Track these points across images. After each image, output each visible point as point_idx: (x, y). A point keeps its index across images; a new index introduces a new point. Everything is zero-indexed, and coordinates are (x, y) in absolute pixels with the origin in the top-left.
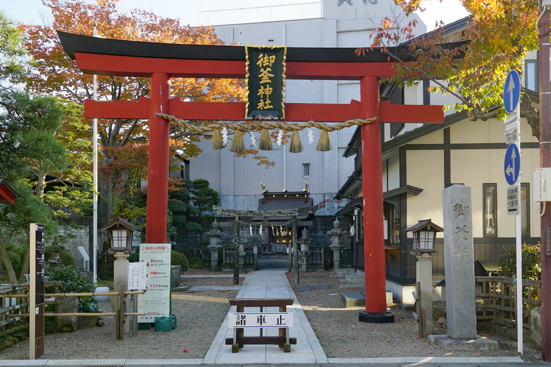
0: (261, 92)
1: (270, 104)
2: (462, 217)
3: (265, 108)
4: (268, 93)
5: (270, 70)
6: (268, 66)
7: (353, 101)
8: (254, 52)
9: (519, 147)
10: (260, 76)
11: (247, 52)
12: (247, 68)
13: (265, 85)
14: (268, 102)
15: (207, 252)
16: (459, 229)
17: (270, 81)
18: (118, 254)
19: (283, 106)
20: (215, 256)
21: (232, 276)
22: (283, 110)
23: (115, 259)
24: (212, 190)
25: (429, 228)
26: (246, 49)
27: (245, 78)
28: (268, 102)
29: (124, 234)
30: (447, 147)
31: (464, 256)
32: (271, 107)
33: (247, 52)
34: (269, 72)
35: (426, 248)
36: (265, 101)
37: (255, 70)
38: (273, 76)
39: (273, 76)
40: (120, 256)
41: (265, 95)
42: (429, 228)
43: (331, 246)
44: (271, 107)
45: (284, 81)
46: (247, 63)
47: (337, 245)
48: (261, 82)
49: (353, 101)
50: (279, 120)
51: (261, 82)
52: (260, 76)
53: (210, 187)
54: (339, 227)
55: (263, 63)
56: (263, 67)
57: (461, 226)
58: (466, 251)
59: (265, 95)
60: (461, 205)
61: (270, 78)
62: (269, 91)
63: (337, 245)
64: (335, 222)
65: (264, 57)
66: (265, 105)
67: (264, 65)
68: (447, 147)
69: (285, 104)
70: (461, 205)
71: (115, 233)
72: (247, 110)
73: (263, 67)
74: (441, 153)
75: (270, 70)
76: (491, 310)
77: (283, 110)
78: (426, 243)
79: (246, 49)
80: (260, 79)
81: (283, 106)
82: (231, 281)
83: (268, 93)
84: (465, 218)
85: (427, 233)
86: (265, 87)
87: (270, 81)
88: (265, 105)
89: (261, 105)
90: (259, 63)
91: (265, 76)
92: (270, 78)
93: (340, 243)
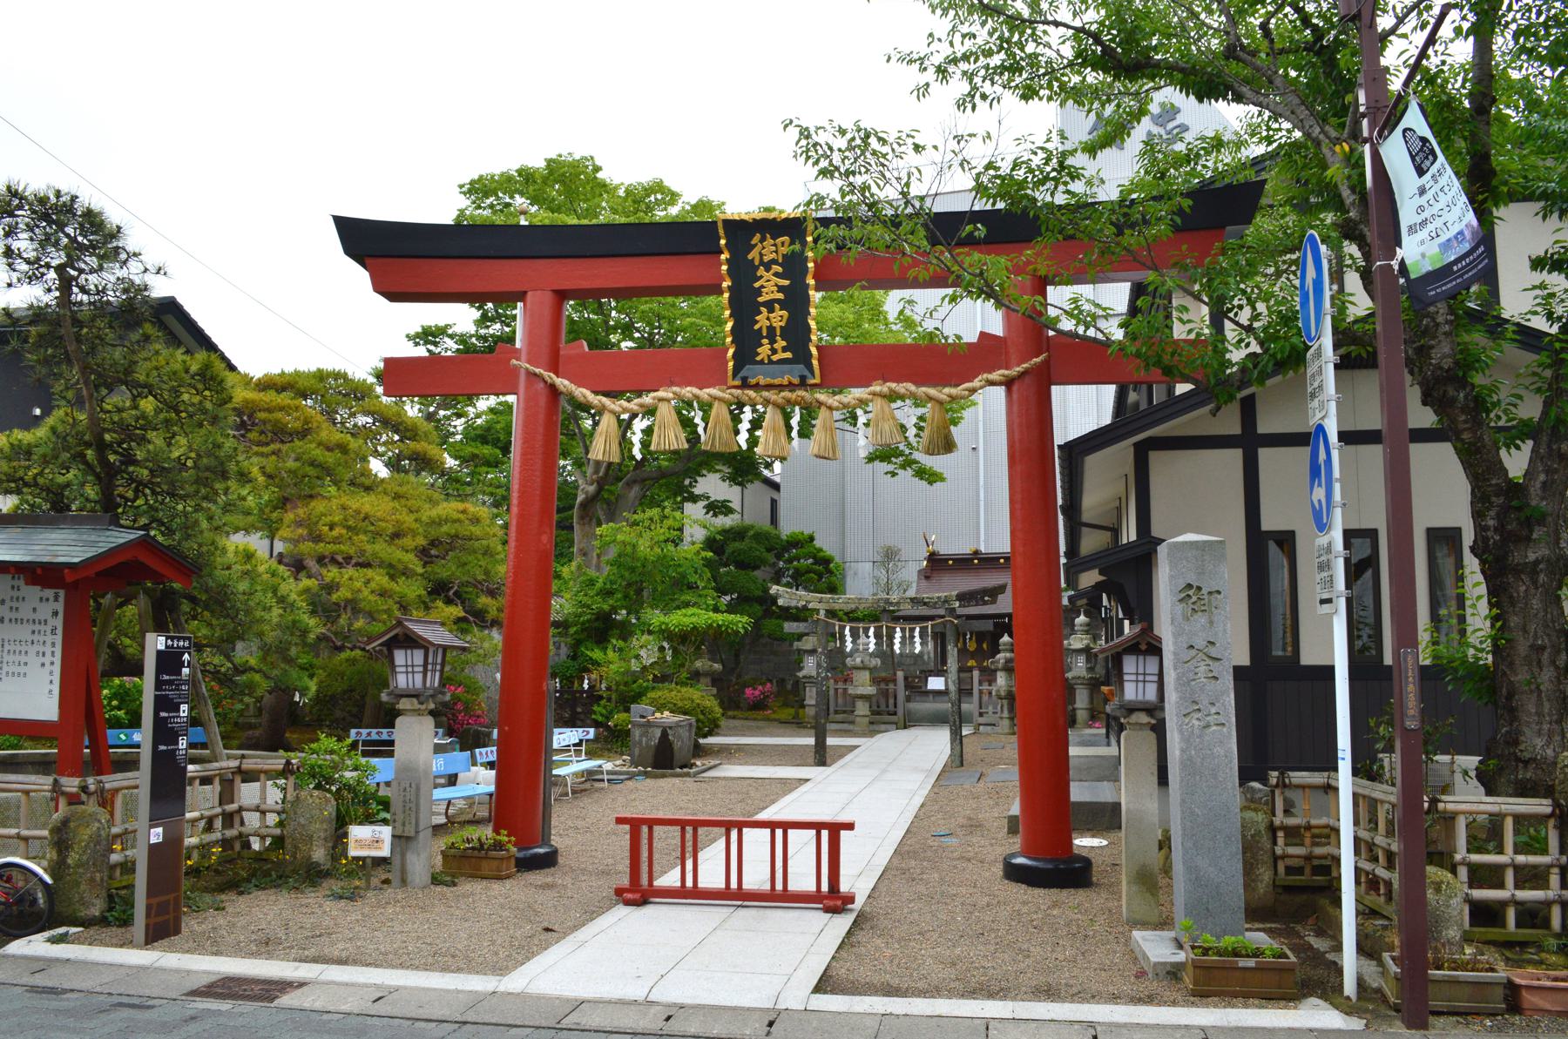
0: (762, 321)
1: (784, 350)
2: (1201, 619)
3: (775, 358)
4: (778, 324)
5: (780, 269)
6: (774, 262)
7: (982, 334)
8: (743, 231)
9: (1333, 437)
10: (757, 285)
11: (721, 232)
12: (724, 268)
13: (770, 305)
14: (780, 344)
15: (798, 687)
16: (1193, 652)
17: (781, 296)
18: (404, 704)
19: (814, 351)
20: (811, 696)
21: (811, 741)
22: (815, 362)
23: (399, 713)
24: (821, 550)
25: (1143, 647)
26: (720, 225)
27: (720, 292)
28: (780, 344)
29: (418, 656)
30: (1250, 442)
31: (1208, 726)
32: (788, 355)
33: (721, 232)
34: (776, 274)
35: (1140, 698)
36: (773, 342)
37: (744, 274)
38: (787, 283)
39: (787, 283)
40: (409, 707)
41: (771, 329)
42: (1143, 647)
43: (1069, 675)
44: (788, 355)
45: (811, 292)
46: (723, 257)
47: (1084, 673)
48: (760, 299)
49: (982, 334)
50: (803, 383)
51: (760, 299)
52: (757, 285)
53: (817, 543)
54: (1087, 632)
55: (761, 255)
56: (762, 263)
57: (1200, 643)
58: (1213, 710)
59: (771, 329)
60: (1199, 588)
61: (781, 289)
62: (779, 318)
63: (1084, 673)
64: (1077, 621)
65: (763, 240)
66: (774, 351)
67: (766, 259)
68: (1250, 442)
69: (818, 348)
70: (1199, 588)
71: (400, 657)
72: (731, 364)
73: (762, 263)
74: (1235, 456)
75: (780, 269)
76: (1323, 862)
77: (815, 362)
78: (1141, 685)
79: (720, 225)
80: (759, 292)
81: (814, 351)
82: (811, 756)
83: (778, 324)
84: (1211, 622)
85: (1141, 658)
86: (771, 310)
87: (781, 296)
88: (774, 351)
89: (764, 351)
90: (753, 255)
91: (770, 285)
92: (781, 289)
93: (1090, 670)
